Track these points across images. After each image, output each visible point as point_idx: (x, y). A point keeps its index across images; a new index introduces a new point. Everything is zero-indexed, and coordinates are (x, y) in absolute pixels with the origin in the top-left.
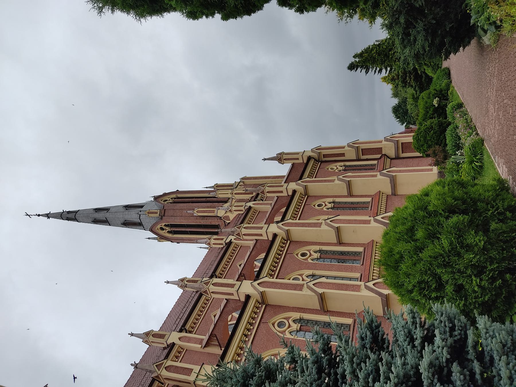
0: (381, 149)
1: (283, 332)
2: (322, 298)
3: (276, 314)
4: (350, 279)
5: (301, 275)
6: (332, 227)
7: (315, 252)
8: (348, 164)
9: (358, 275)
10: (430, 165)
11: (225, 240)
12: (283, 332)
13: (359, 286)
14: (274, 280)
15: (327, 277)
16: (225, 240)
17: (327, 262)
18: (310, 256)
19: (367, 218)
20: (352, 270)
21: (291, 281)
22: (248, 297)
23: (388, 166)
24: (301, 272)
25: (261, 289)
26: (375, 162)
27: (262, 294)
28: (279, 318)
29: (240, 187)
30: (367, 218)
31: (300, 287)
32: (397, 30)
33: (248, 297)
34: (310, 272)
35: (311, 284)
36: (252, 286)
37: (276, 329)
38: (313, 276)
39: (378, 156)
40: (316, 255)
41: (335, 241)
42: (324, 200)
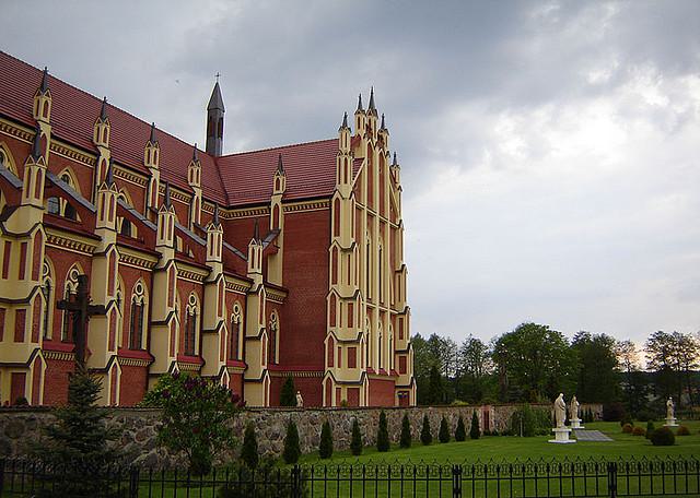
0: (405, 373)
1: (69, 278)
4: (46, 328)
6: (261, 334)
7: (142, 301)
8: (198, 320)
9: (50, 337)
11: (43, 119)
12: (69, 278)
14: (44, 244)
16: (43, 119)
19: (118, 343)
20: (56, 326)
21: (42, 263)
23: (125, 362)
26: (240, 358)
30: (176, 352)
33: (99, 239)
34: (53, 285)
35: (39, 291)
38: (49, 287)
39: (398, 371)
40: (191, 311)
41: (205, 329)
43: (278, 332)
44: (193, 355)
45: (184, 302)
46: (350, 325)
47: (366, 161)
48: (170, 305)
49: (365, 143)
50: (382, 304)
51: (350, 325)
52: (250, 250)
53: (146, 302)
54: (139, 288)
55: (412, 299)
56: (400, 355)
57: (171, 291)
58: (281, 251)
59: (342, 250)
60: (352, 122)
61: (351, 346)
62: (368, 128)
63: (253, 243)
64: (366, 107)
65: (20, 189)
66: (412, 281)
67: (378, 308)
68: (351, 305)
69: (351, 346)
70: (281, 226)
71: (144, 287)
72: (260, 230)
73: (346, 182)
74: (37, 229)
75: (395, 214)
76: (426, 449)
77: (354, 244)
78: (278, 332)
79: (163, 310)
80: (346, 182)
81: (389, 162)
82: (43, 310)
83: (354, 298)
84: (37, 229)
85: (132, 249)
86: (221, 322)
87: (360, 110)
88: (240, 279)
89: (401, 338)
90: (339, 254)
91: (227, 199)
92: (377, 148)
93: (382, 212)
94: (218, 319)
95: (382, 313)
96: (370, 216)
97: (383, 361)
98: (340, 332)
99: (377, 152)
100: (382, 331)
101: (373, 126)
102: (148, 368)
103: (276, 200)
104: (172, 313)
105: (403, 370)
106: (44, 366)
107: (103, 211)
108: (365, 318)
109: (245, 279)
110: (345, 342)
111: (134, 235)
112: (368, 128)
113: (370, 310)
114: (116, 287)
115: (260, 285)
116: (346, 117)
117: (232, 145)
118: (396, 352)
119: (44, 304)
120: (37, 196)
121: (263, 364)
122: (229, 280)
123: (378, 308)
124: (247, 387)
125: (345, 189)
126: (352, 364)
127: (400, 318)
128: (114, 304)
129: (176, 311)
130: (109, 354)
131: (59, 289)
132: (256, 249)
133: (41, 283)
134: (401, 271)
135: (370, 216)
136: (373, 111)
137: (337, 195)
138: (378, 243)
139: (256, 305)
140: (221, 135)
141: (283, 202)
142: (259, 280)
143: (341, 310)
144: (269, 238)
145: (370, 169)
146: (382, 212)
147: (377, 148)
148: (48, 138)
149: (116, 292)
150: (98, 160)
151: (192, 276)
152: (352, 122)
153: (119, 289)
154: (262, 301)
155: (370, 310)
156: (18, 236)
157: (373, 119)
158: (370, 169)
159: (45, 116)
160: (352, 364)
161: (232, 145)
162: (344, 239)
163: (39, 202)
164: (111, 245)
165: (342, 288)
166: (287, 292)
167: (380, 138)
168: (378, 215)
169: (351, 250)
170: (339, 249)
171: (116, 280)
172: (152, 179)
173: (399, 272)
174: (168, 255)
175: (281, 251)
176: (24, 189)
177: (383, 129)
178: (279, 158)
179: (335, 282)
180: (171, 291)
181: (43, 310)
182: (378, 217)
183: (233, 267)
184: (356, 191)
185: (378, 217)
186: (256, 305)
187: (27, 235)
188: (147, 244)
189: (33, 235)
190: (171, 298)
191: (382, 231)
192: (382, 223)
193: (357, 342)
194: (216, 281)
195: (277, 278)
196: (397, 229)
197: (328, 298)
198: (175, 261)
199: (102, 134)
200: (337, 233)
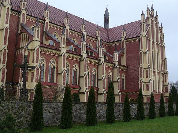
0: (149, 90)
1: (74, 67)
2: (83, 77)
3: (55, 59)
5: (68, 66)
9: (159, 90)
10: (67, 84)
11: (84, 30)
13: (87, 87)
15: (88, 78)
16: (47, 17)
17: (92, 77)
18: (75, 68)
19: (105, 87)
21: (66, 63)
22: (60, 51)
24: (69, 66)
25: (63, 55)
26: (78, 84)
27: (61, 55)
28: (55, 61)
29: (27, 36)
31: (64, 67)
32: (64, 67)
36: (85, 57)
37: (75, 65)
39: (165, 91)
42: (78, 68)
43: (125, 80)
44: (76, 85)
45: (108, 73)
46: (147, 77)
47: (151, 25)
48: (103, 74)
49: (150, 19)
50: (158, 70)
51: (147, 77)
52: (114, 54)
53: (112, 76)
54: (76, 66)
55: (169, 69)
56: (166, 86)
57: (85, 67)
58: (125, 55)
59: (144, 53)
60: (145, 13)
61: (147, 84)
62: (151, 15)
63: (115, 52)
64: (150, 9)
65: (98, 53)
66: (168, 62)
67: (157, 71)
68: (147, 71)
69: (147, 84)
70: (125, 47)
71: (77, 66)
72: (119, 49)
73: (144, 32)
74: (64, 54)
75: (162, 42)
76: (140, 123)
77: (147, 51)
78: (125, 80)
79: (83, 73)
80: (144, 32)
81: (160, 26)
82: (88, 79)
83: (148, 68)
84: (64, 54)
85: (75, 54)
86: (118, 79)
87: (148, 10)
88: (57, 50)
89: (166, 81)
90: (143, 54)
91: (109, 40)
92: (155, 21)
93: (157, 41)
94: (118, 78)
95: (159, 73)
96: (153, 42)
97: (159, 89)
98: (144, 79)
99: (155, 22)
100: (158, 79)
101: (153, 15)
102: (79, 91)
103: (123, 39)
104: (103, 76)
105: (167, 91)
106: (121, 95)
107: (100, 53)
108: (152, 75)
109: (113, 63)
110: (145, 82)
111: (94, 55)
112: (151, 15)
113: (154, 72)
114: (105, 73)
115: (117, 65)
116: (161, 24)
117: (112, 25)
118: (164, 86)
119: (88, 77)
120: (64, 44)
121: (119, 90)
122: (106, 63)
123: (157, 71)
124: (99, 96)
125: (144, 34)
126: (148, 89)
127: (165, 75)
128: (104, 77)
129: (105, 76)
130: (103, 90)
131: (71, 70)
132: (116, 54)
133: (87, 72)
134: (165, 60)
135: (153, 42)
136: (153, 10)
137: (141, 36)
138: (156, 51)
139: (116, 71)
140: (108, 23)
141: (125, 39)
142: (117, 63)
143: (144, 72)
144: (121, 51)
145: (153, 28)
146: (157, 41)
147: (155, 21)
148: (68, 29)
149: (104, 74)
150: (44, 22)
151: (110, 66)
152: (145, 13)
153: (105, 73)
154: (118, 70)
155: (154, 72)
156: (32, 50)
157: (153, 12)
158: (153, 28)
159: (84, 30)
160: (148, 89)
161: (112, 25)
162: (144, 49)
163: (65, 46)
164: (85, 57)
165: (144, 65)
166: (127, 67)
167: (156, 18)
168: (156, 42)
169: (146, 53)
170: (142, 52)
171: (104, 71)
172: (98, 40)
173: (164, 60)
174: (85, 55)
175: (125, 55)
176: (34, 36)
177: (157, 15)
178: (124, 27)
179: (141, 63)
180: (85, 67)
181: (88, 79)
182: (156, 43)
183: (109, 60)
184: (148, 34)
185: (156, 43)
186: (116, 71)
187: (34, 49)
188: (77, 51)
189: (36, 49)
190: (85, 69)
191: (158, 47)
192: (158, 45)
193: (149, 82)
194: (102, 64)
195: (124, 63)
196: (163, 47)
197: (140, 68)
198: (87, 57)
199: (67, 22)
200: (142, 48)
